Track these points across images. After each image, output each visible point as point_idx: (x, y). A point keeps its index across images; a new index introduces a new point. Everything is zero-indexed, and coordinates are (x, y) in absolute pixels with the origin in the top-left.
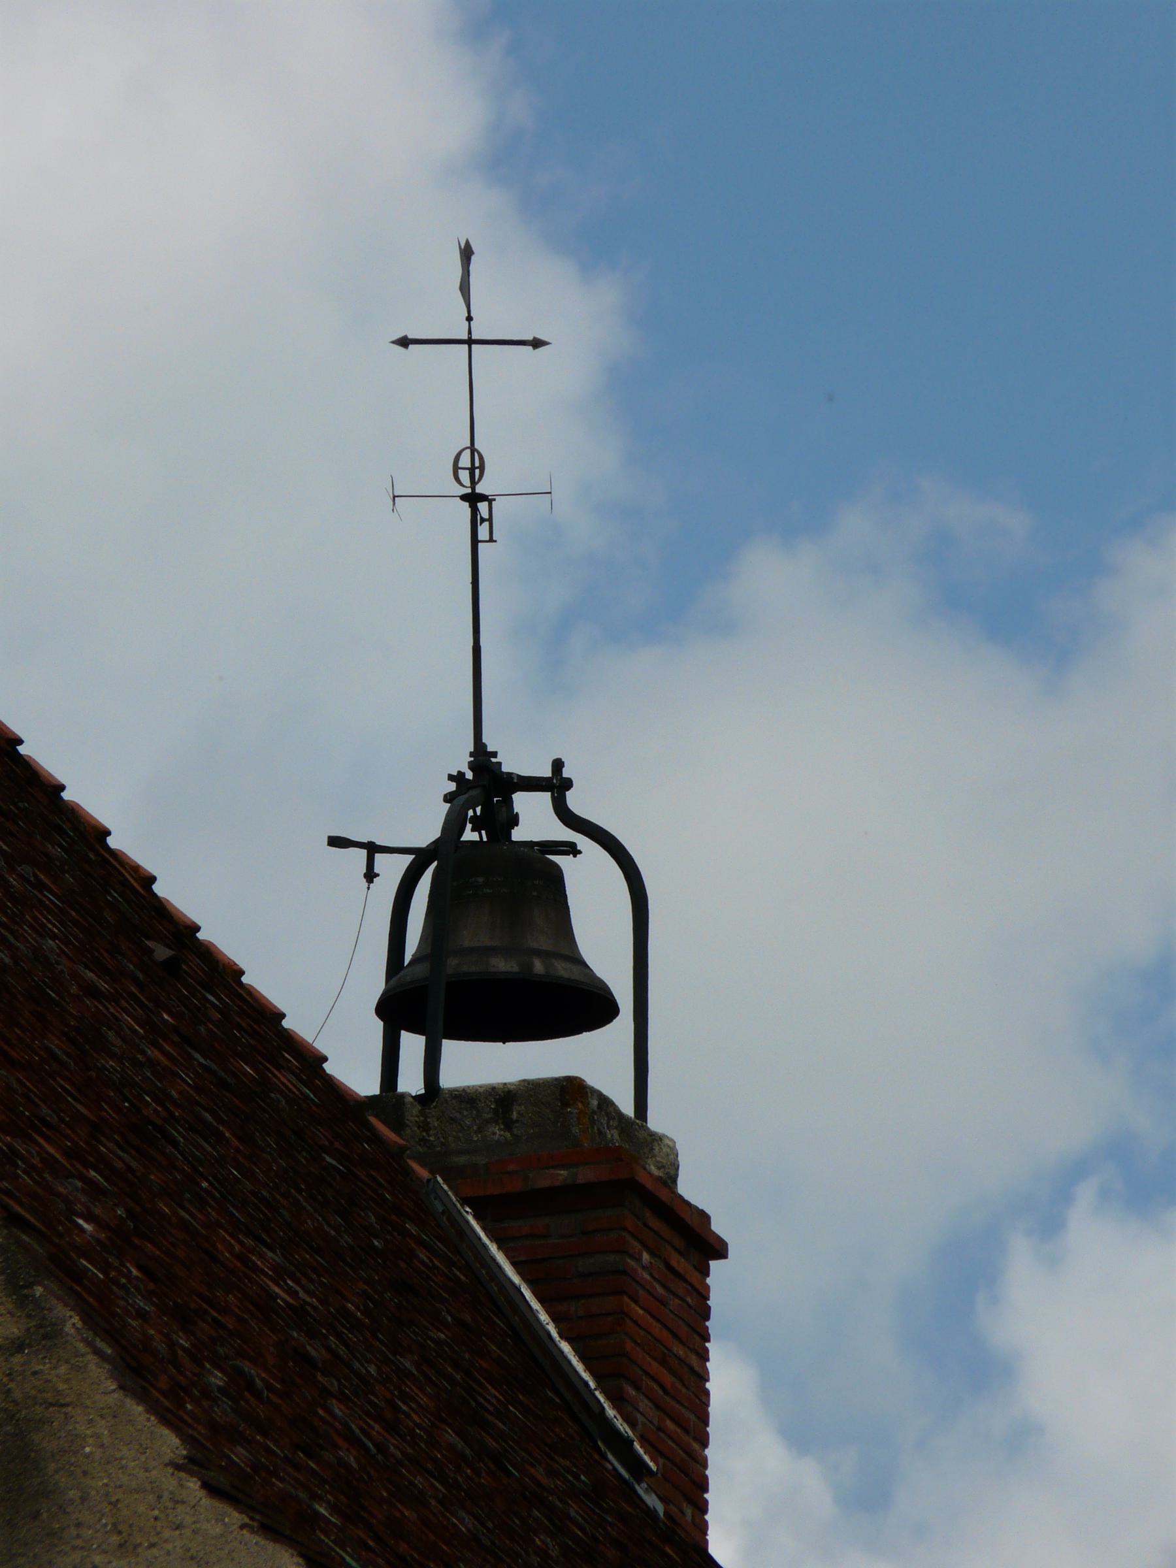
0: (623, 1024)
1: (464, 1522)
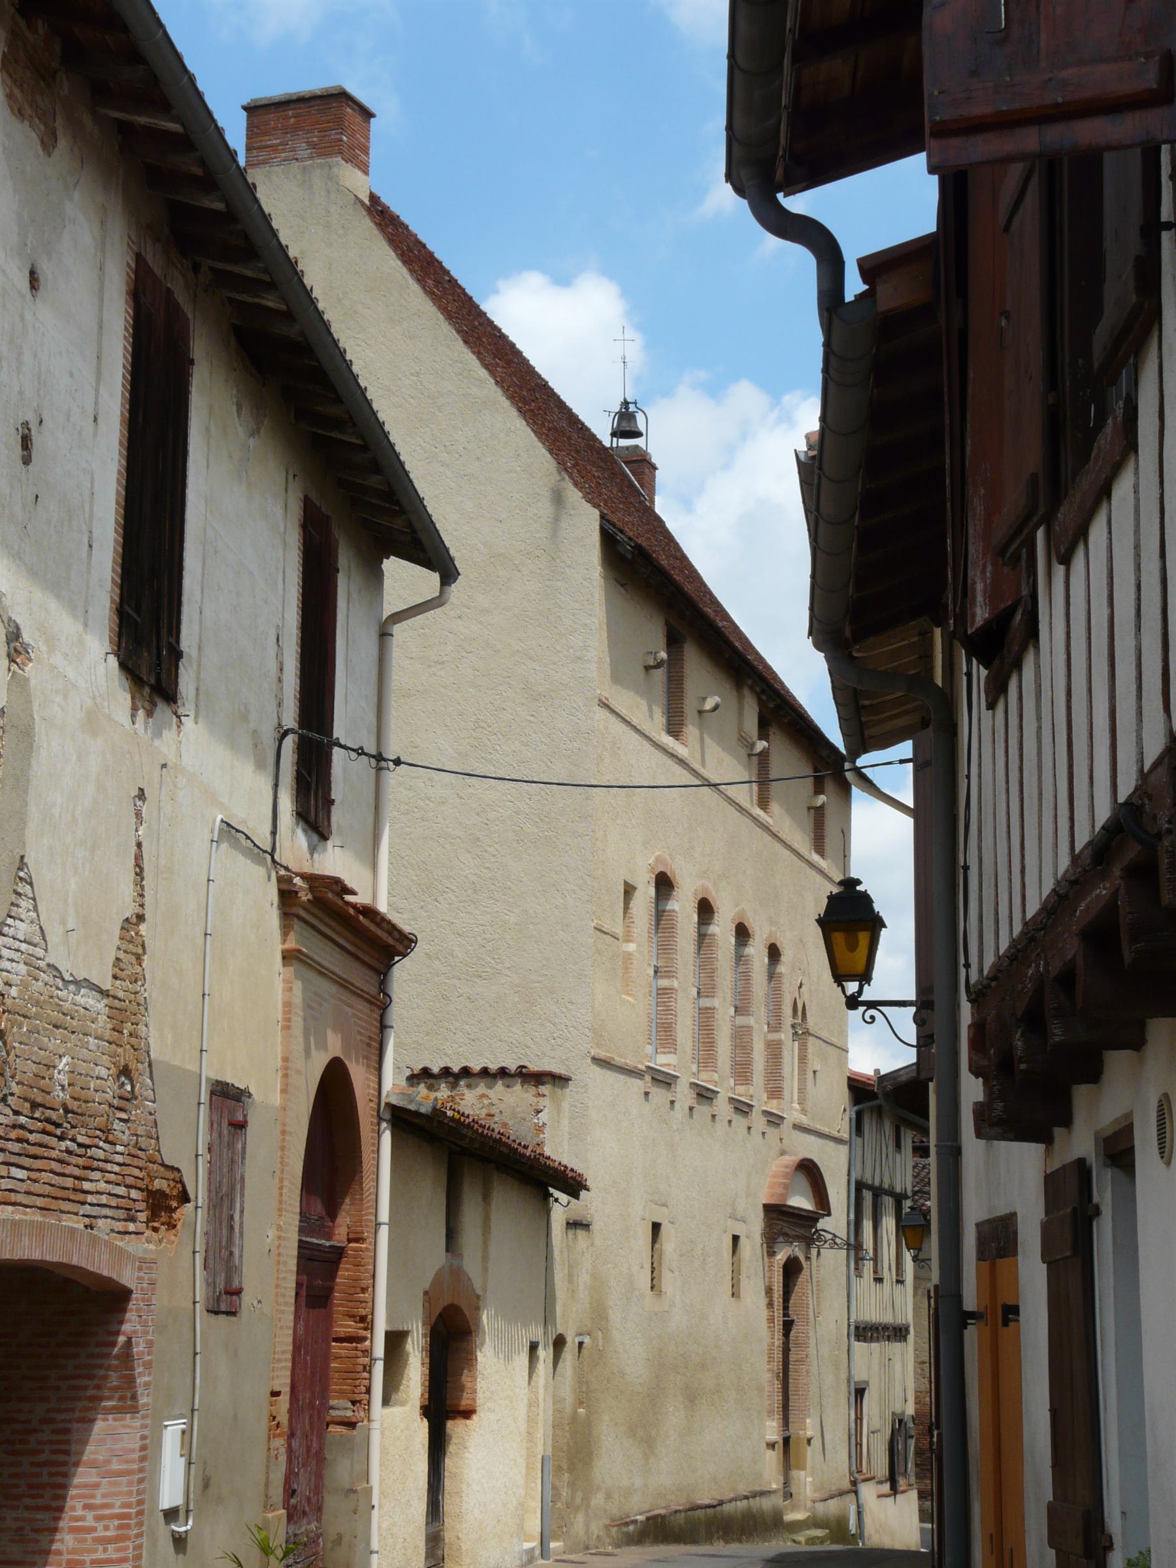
0: (644, 436)
1: (621, 506)
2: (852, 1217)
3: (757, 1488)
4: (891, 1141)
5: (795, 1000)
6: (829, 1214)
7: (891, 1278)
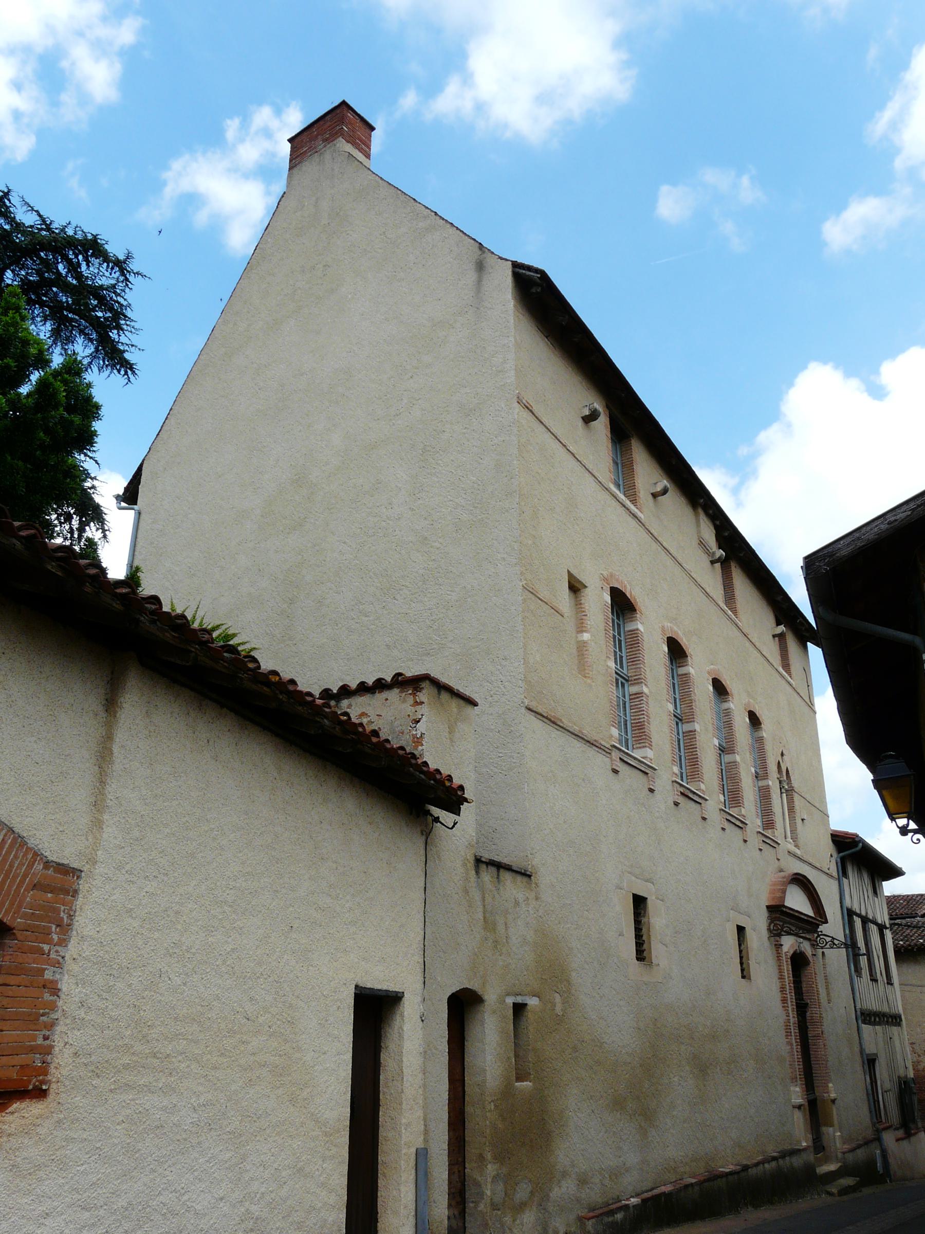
2: (847, 932)
3: (787, 1147)
4: (869, 886)
5: (779, 762)
6: (826, 922)
7: (883, 980)
